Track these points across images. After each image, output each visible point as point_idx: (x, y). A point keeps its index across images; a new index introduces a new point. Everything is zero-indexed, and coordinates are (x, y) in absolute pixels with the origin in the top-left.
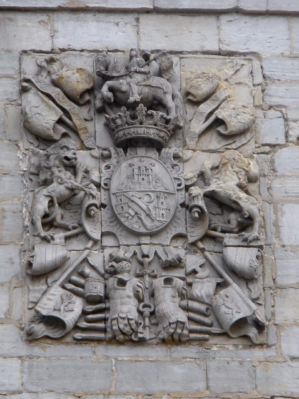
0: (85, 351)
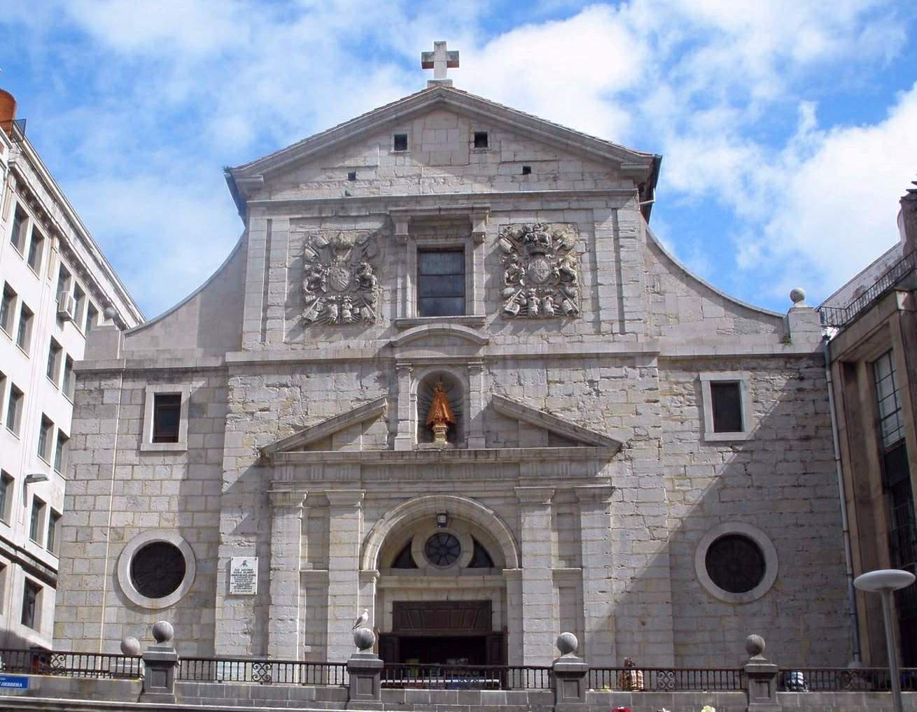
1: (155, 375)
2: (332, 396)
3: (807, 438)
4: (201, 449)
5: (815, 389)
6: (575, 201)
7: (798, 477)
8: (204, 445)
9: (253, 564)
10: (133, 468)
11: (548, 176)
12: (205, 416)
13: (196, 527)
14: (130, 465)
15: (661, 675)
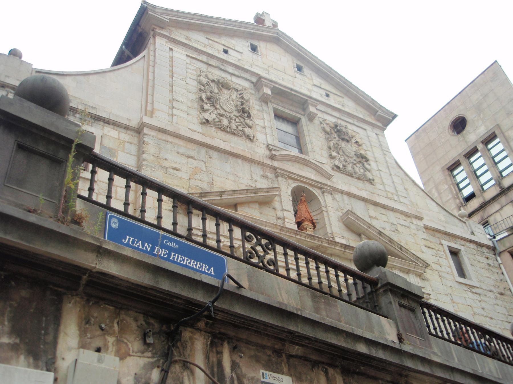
0: (343, 175)
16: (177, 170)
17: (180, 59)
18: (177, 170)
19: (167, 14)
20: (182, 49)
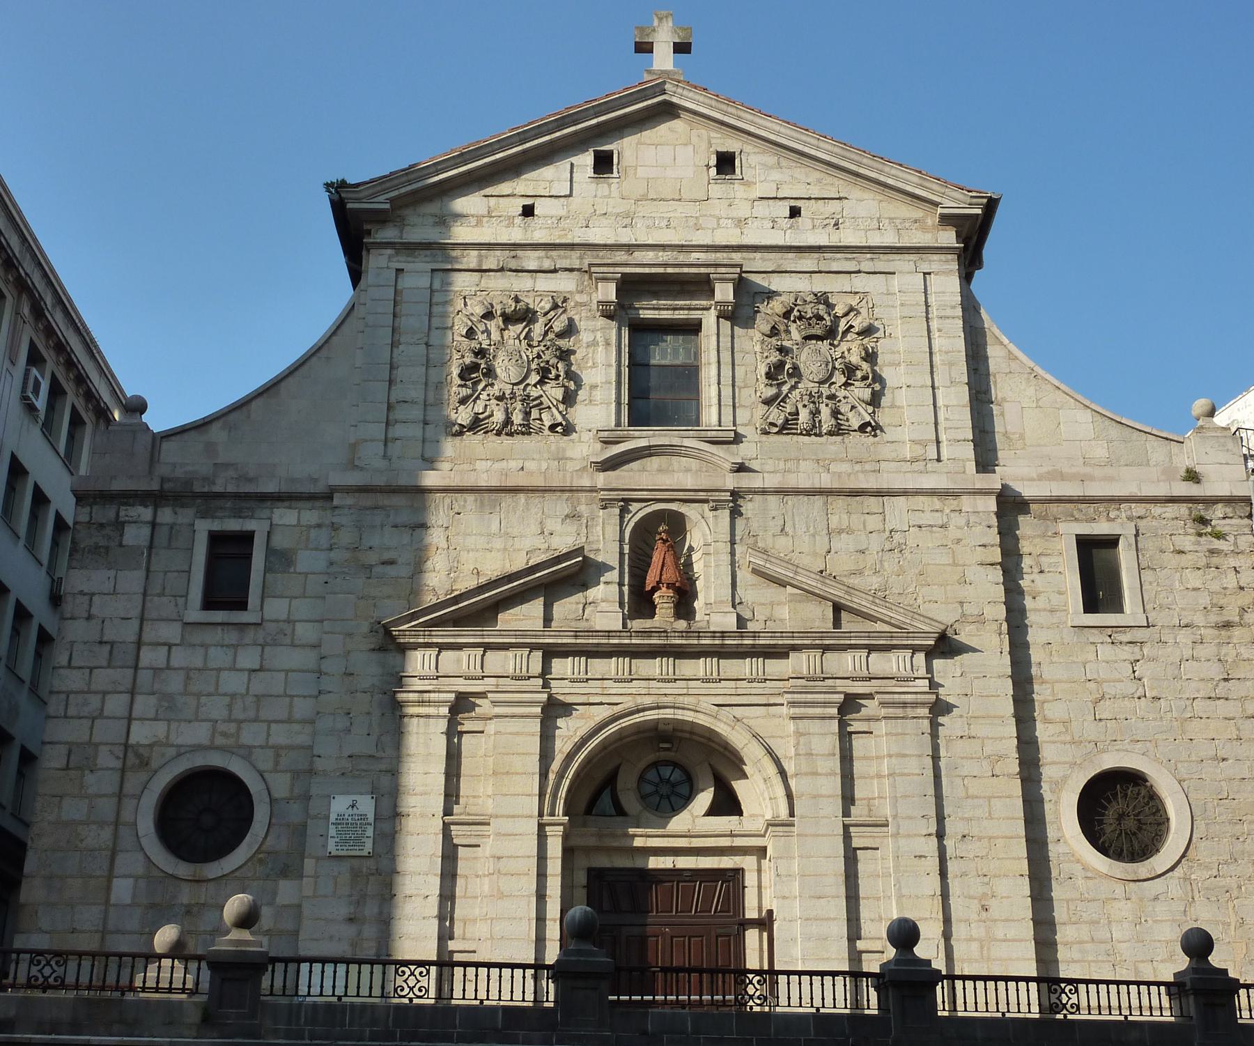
1: (209, 501)
2: (498, 544)
3: (1227, 625)
4: (284, 621)
5: (1236, 550)
6: (868, 259)
7: (1217, 685)
8: (289, 614)
9: (366, 805)
10: (169, 651)
11: (827, 221)
12: (292, 570)
13: (272, 747)
14: (164, 644)
15: (403, 972)
16: (392, 562)
17: (418, 288)
18: (392, 562)
19: (388, 189)
20: (424, 259)
